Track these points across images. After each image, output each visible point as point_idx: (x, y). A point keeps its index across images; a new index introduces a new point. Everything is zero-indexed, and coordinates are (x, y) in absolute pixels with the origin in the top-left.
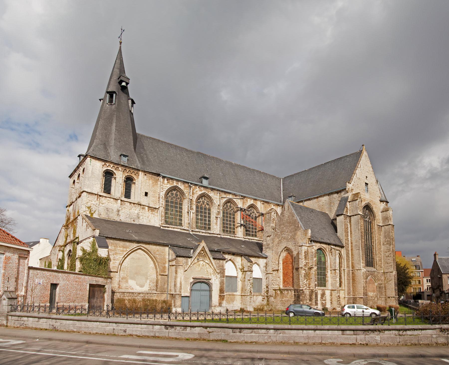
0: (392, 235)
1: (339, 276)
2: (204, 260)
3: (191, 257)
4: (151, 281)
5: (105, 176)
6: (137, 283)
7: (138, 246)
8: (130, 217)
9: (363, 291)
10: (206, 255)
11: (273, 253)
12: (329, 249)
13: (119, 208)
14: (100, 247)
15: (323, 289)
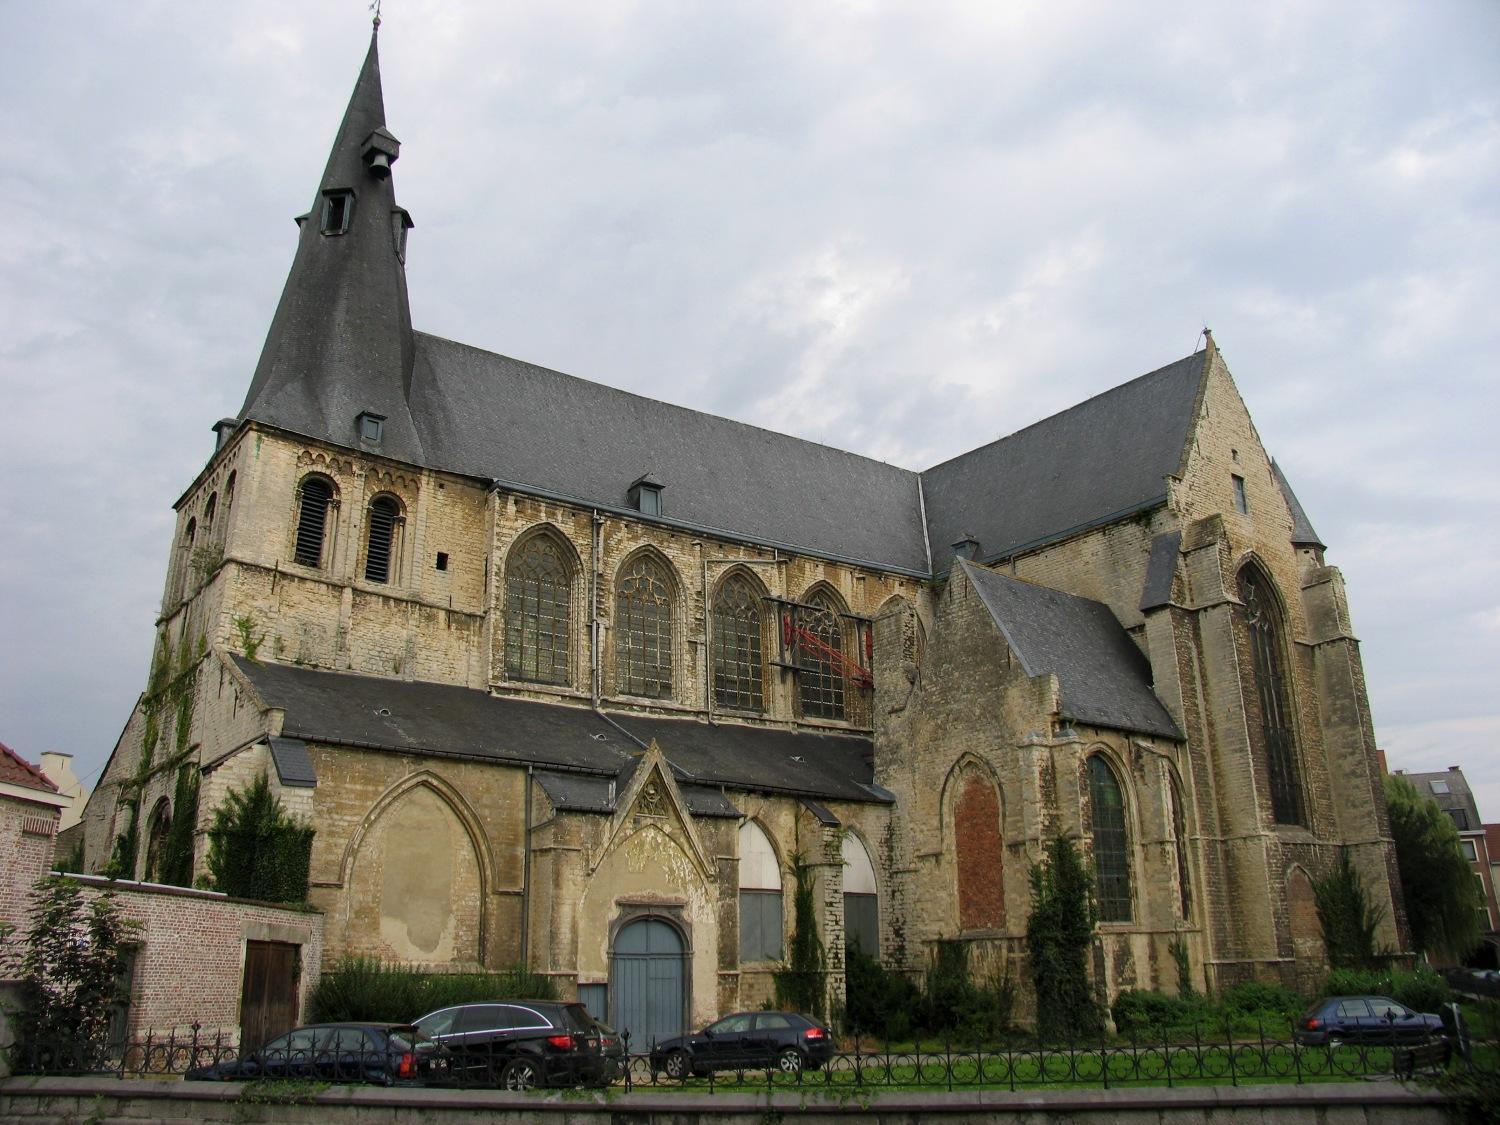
0: (1356, 684)
1: (1177, 870)
2: (659, 825)
4: (461, 921)
5: (304, 497)
6: (409, 933)
7: (418, 775)
9: (1275, 932)
11: (914, 782)
12: (1130, 752)
14: (285, 781)
15: (1122, 930)
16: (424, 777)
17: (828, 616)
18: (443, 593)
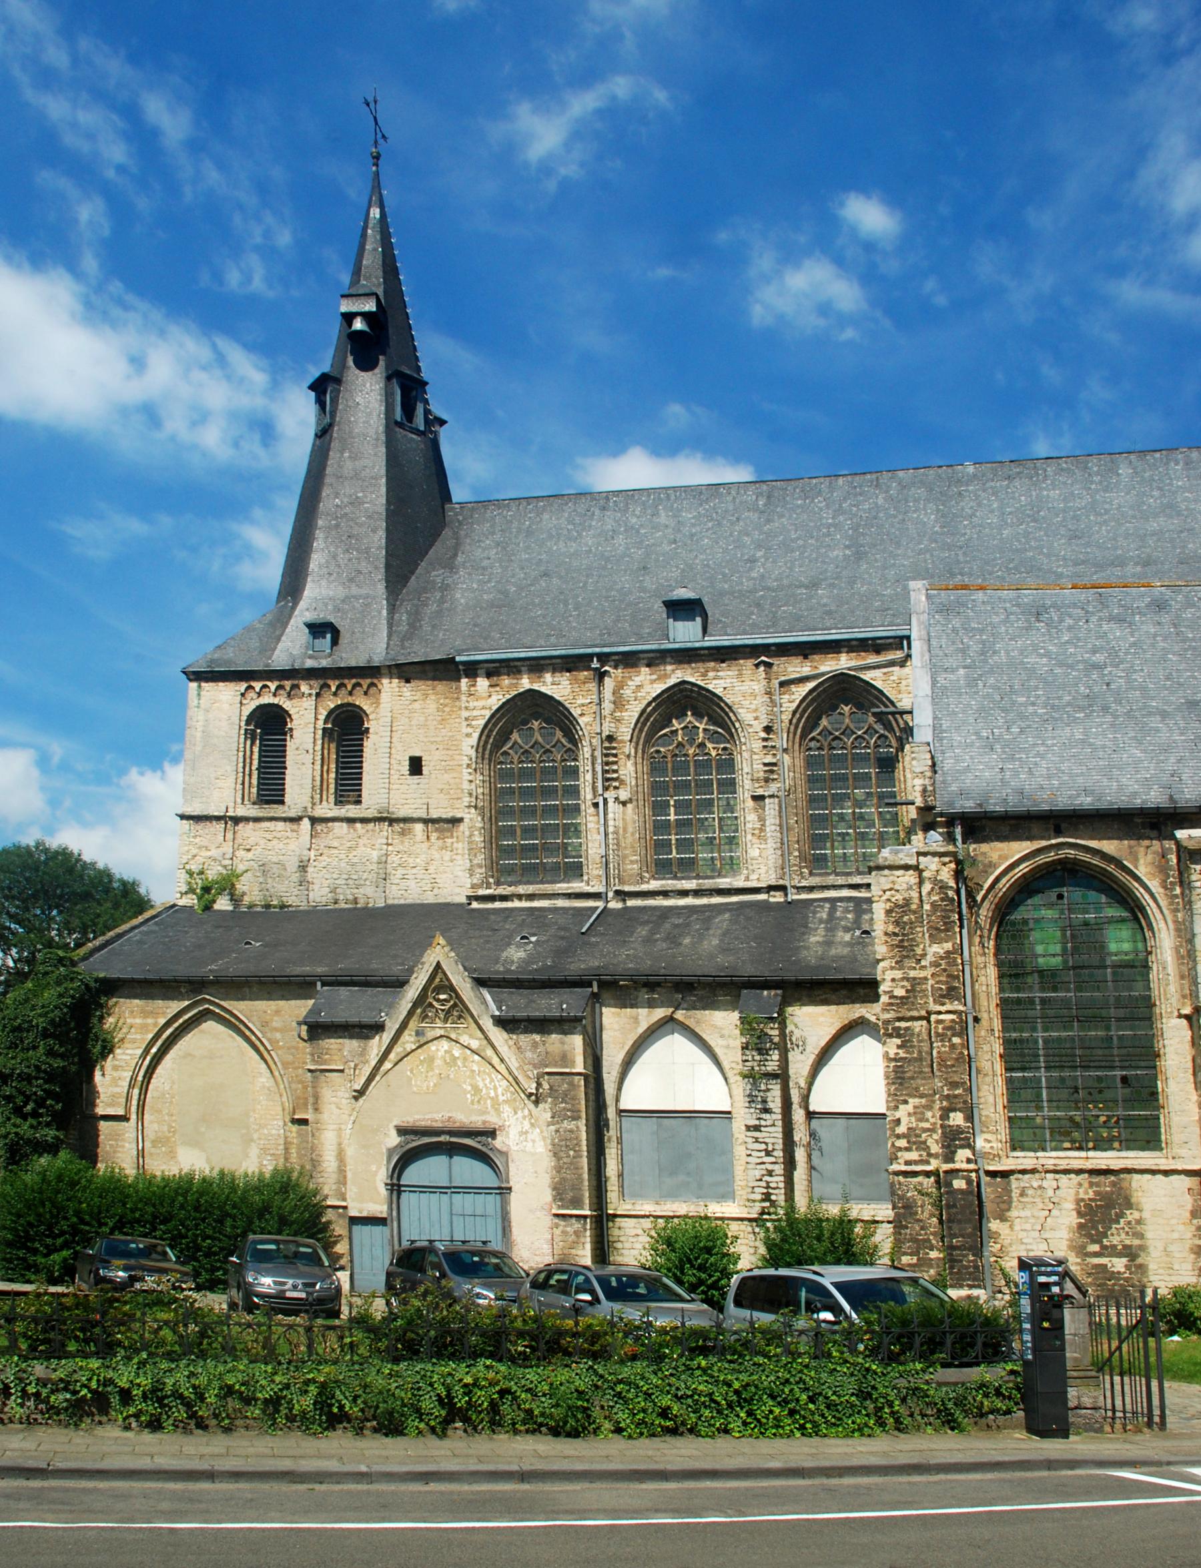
2: (453, 1036)
3: (379, 1028)
4: (264, 1150)
8: (350, 882)
10: (457, 1010)
13: (306, 852)
18: (419, 801)
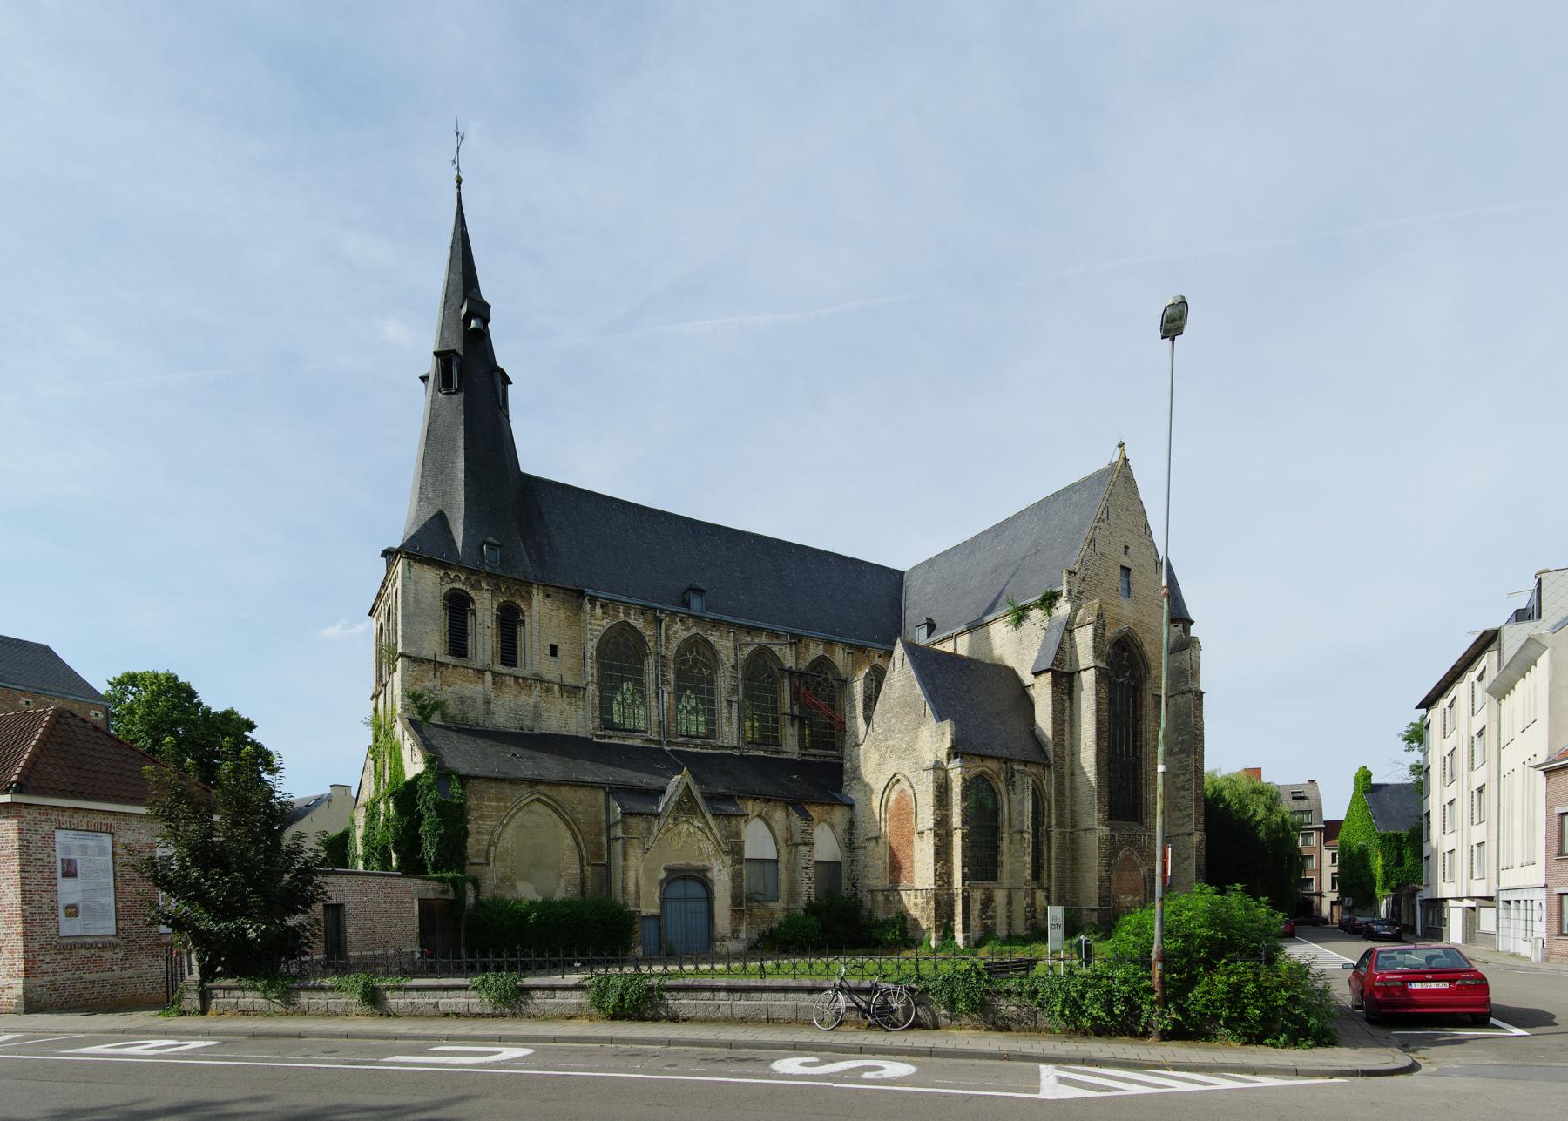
0: (1196, 725)
2: (691, 821)
4: (568, 882)
5: (450, 607)
6: (536, 890)
12: (1007, 773)
16: (537, 796)
17: (826, 680)
